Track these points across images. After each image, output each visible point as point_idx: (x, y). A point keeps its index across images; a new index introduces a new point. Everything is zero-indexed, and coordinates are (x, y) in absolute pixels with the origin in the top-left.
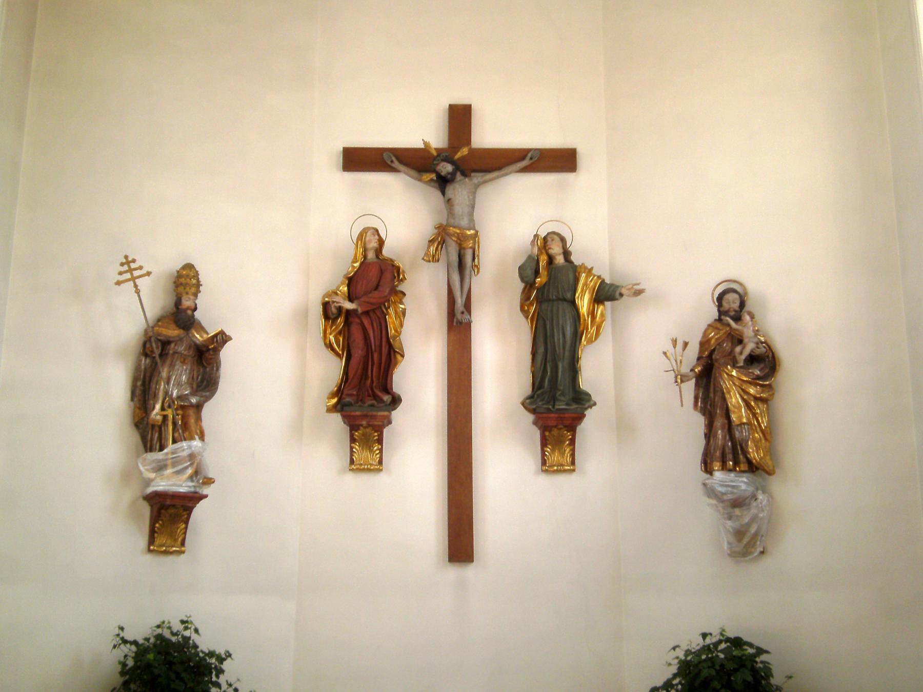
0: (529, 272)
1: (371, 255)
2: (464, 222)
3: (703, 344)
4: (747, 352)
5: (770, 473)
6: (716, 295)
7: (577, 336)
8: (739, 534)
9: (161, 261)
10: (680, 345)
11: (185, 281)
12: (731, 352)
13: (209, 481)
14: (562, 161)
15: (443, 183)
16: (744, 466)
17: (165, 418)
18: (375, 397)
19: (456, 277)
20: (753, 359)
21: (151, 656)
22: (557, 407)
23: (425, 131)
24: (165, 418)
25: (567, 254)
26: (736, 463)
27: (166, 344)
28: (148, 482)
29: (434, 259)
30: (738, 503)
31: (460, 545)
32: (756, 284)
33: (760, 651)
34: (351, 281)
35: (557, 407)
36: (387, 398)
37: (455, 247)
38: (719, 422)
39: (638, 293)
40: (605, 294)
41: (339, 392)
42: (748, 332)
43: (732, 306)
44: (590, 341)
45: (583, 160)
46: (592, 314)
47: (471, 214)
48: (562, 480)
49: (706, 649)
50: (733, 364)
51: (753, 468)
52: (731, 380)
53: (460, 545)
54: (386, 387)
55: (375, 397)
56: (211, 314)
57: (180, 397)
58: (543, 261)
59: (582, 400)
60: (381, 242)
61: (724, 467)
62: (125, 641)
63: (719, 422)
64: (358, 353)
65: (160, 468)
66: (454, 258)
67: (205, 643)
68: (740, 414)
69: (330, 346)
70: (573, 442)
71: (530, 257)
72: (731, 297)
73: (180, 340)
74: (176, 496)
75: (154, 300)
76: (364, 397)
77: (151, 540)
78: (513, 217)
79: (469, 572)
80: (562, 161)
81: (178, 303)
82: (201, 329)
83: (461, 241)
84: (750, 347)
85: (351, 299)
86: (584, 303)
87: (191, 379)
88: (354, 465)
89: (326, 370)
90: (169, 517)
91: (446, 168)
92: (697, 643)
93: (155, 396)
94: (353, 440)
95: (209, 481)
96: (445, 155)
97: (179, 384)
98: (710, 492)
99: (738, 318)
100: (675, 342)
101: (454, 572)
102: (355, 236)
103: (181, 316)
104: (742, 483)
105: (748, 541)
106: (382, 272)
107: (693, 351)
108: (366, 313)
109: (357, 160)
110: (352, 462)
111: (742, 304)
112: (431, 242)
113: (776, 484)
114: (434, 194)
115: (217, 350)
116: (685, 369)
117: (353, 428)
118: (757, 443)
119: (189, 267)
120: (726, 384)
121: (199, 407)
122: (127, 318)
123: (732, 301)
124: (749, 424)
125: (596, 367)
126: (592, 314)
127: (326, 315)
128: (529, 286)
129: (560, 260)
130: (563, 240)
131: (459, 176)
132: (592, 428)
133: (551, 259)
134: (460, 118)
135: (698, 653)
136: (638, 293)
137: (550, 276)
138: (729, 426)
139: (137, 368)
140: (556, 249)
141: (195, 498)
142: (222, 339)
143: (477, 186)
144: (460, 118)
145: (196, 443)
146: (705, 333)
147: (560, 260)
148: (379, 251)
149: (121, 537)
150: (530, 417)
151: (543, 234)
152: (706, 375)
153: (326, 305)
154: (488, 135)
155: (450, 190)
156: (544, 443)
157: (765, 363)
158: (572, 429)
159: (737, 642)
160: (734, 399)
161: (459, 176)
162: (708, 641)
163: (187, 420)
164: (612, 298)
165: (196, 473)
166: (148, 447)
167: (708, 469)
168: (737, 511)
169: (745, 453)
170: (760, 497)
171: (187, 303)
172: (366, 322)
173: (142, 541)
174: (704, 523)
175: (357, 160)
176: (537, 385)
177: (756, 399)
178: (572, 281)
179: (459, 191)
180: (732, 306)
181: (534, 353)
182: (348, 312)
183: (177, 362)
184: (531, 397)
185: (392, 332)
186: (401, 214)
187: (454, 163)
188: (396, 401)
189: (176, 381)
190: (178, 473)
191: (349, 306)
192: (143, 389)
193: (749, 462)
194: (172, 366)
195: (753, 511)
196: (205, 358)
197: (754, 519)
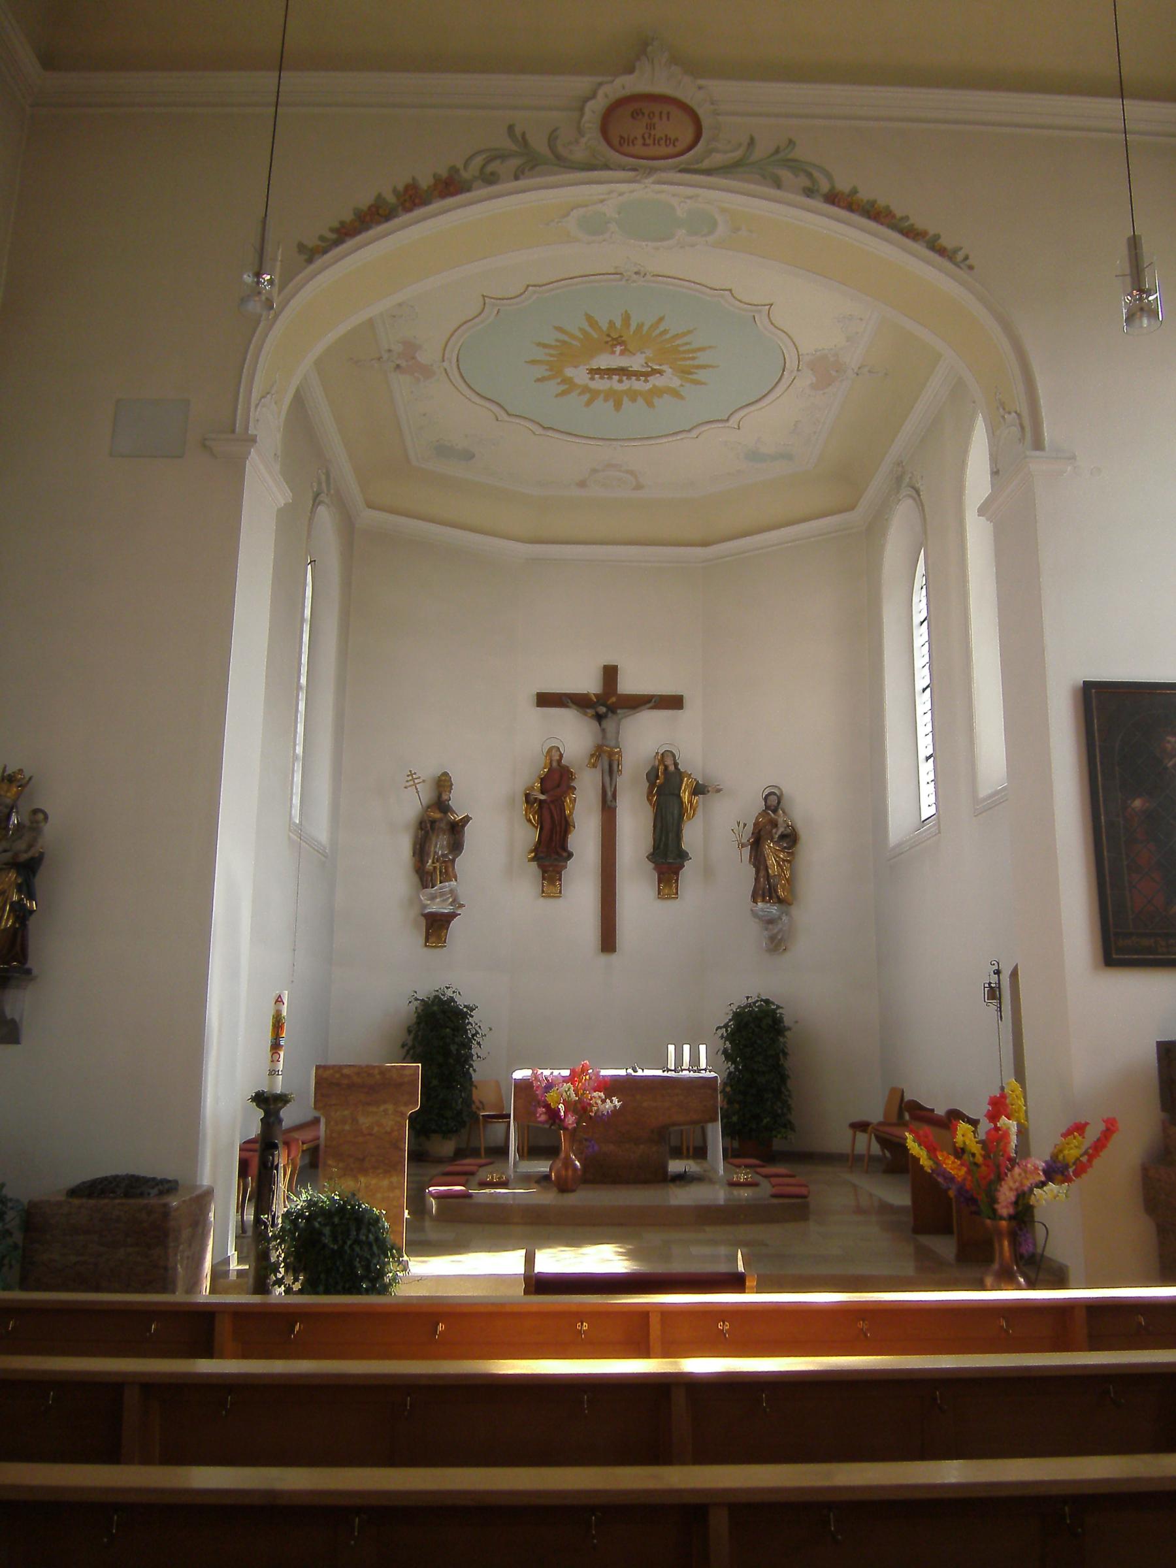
0: (652, 776)
1: (555, 764)
2: (613, 743)
3: (756, 824)
4: (779, 833)
5: (790, 904)
6: (766, 793)
7: (681, 816)
8: (772, 938)
9: (428, 770)
10: (741, 825)
11: (443, 783)
12: (771, 832)
13: (462, 906)
14: (674, 702)
15: (599, 718)
16: (775, 900)
17: (435, 868)
18: (557, 853)
19: (607, 779)
20: (783, 837)
21: (435, 1008)
22: (667, 859)
23: (590, 685)
24: (435, 868)
25: (676, 764)
26: (771, 898)
27: (433, 822)
28: (425, 906)
29: (594, 766)
30: (771, 921)
31: (608, 941)
32: (787, 789)
33: (778, 1007)
34: (543, 781)
35: (667, 859)
36: (565, 854)
37: (606, 758)
38: (762, 873)
39: (719, 791)
40: (699, 790)
41: (536, 850)
42: (780, 820)
43: (774, 802)
44: (689, 819)
45: (686, 702)
46: (690, 802)
47: (617, 738)
48: (669, 903)
49: (749, 1005)
50: (773, 836)
51: (780, 901)
52: (769, 847)
53: (608, 941)
54: (563, 845)
55: (557, 853)
56: (461, 803)
57: (443, 855)
58: (661, 768)
59: (683, 856)
60: (561, 756)
61: (763, 901)
62: (416, 999)
63: (762, 873)
64: (547, 826)
65: (433, 898)
66: (606, 767)
67: (461, 1002)
68: (774, 870)
69: (529, 821)
70: (677, 881)
71: (653, 767)
72: (773, 798)
73: (441, 819)
74: (443, 914)
75: (426, 794)
76: (551, 853)
77: (427, 940)
78: (643, 738)
79: (614, 957)
80: (674, 702)
81: (440, 796)
82: (453, 812)
83: (611, 755)
84: (781, 830)
85: (542, 793)
86: (685, 797)
87: (449, 843)
88: (544, 894)
89: (528, 836)
90: (436, 927)
91: (602, 710)
92: (744, 1002)
93: (428, 855)
94: (544, 878)
95: (462, 906)
96: (602, 699)
97: (442, 848)
98: (754, 914)
99: (775, 811)
100: (739, 823)
101: (604, 958)
102: (545, 751)
103: (441, 804)
104: (774, 909)
105: (777, 943)
106: (561, 776)
107: (750, 828)
108: (552, 802)
109: (545, 700)
110: (543, 892)
111: (779, 802)
112: (592, 756)
113: (795, 911)
114: (595, 723)
115: (464, 826)
116: (744, 840)
117: (544, 872)
118: (783, 887)
119: (445, 774)
120: (767, 851)
121: (453, 861)
122: (410, 806)
123: (773, 800)
124: (779, 875)
125: (692, 835)
126: (690, 802)
127: (527, 801)
128: (652, 785)
129: (672, 768)
130: (674, 756)
131: (610, 714)
132: (689, 873)
133: (666, 767)
134: (610, 674)
135: (745, 1007)
136: (719, 791)
137: (665, 778)
138: (768, 876)
139: (416, 837)
140: (669, 762)
141: (452, 916)
142: (467, 819)
143: (620, 720)
144: (610, 674)
145: (454, 883)
146: (757, 818)
147: (672, 768)
148: (559, 761)
149: (406, 939)
150: (651, 865)
151: (661, 752)
152: (757, 843)
153: (527, 796)
154: (628, 685)
155: (604, 723)
156: (660, 882)
157: (790, 839)
158: (677, 874)
159: (767, 1002)
160: (772, 861)
161: (610, 714)
162: (750, 1000)
163: (448, 873)
164: (703, 793)
165: (454, 901)
166: (425, 886)
167: (755, 901)
168: (770, 926)
169: (776, 892)
170: (784, 918)
171: (445, 797)
172: (552, 806)
173: (422, 940)
174: (753, 932)
175: (545, 700)
176: (656, 847)
177: (784, 861)
178: (676, 816)
179: (609, 724)
180: (774, 802)
181: (655, 826)
182: (541, 801)
183: (438, 834)
184: (652, 854)
185: (567, 812)
186: (573, 736)
187: (607, 704)
188: (570, 855)
189: (439, 845)
190: (444, 901)
191: (542, 797)
192: (420, 851)
193: (778, 897)
194: (438, 836)
195: (780, 926)
196: (456, 830)
197: (780, 931)
